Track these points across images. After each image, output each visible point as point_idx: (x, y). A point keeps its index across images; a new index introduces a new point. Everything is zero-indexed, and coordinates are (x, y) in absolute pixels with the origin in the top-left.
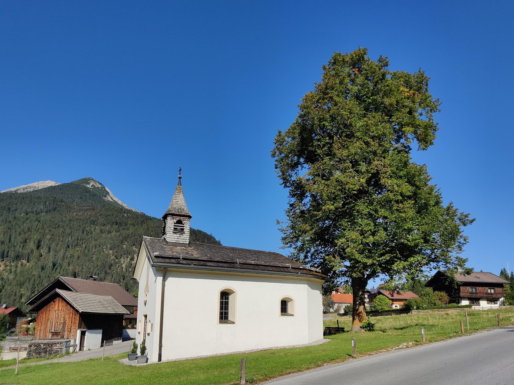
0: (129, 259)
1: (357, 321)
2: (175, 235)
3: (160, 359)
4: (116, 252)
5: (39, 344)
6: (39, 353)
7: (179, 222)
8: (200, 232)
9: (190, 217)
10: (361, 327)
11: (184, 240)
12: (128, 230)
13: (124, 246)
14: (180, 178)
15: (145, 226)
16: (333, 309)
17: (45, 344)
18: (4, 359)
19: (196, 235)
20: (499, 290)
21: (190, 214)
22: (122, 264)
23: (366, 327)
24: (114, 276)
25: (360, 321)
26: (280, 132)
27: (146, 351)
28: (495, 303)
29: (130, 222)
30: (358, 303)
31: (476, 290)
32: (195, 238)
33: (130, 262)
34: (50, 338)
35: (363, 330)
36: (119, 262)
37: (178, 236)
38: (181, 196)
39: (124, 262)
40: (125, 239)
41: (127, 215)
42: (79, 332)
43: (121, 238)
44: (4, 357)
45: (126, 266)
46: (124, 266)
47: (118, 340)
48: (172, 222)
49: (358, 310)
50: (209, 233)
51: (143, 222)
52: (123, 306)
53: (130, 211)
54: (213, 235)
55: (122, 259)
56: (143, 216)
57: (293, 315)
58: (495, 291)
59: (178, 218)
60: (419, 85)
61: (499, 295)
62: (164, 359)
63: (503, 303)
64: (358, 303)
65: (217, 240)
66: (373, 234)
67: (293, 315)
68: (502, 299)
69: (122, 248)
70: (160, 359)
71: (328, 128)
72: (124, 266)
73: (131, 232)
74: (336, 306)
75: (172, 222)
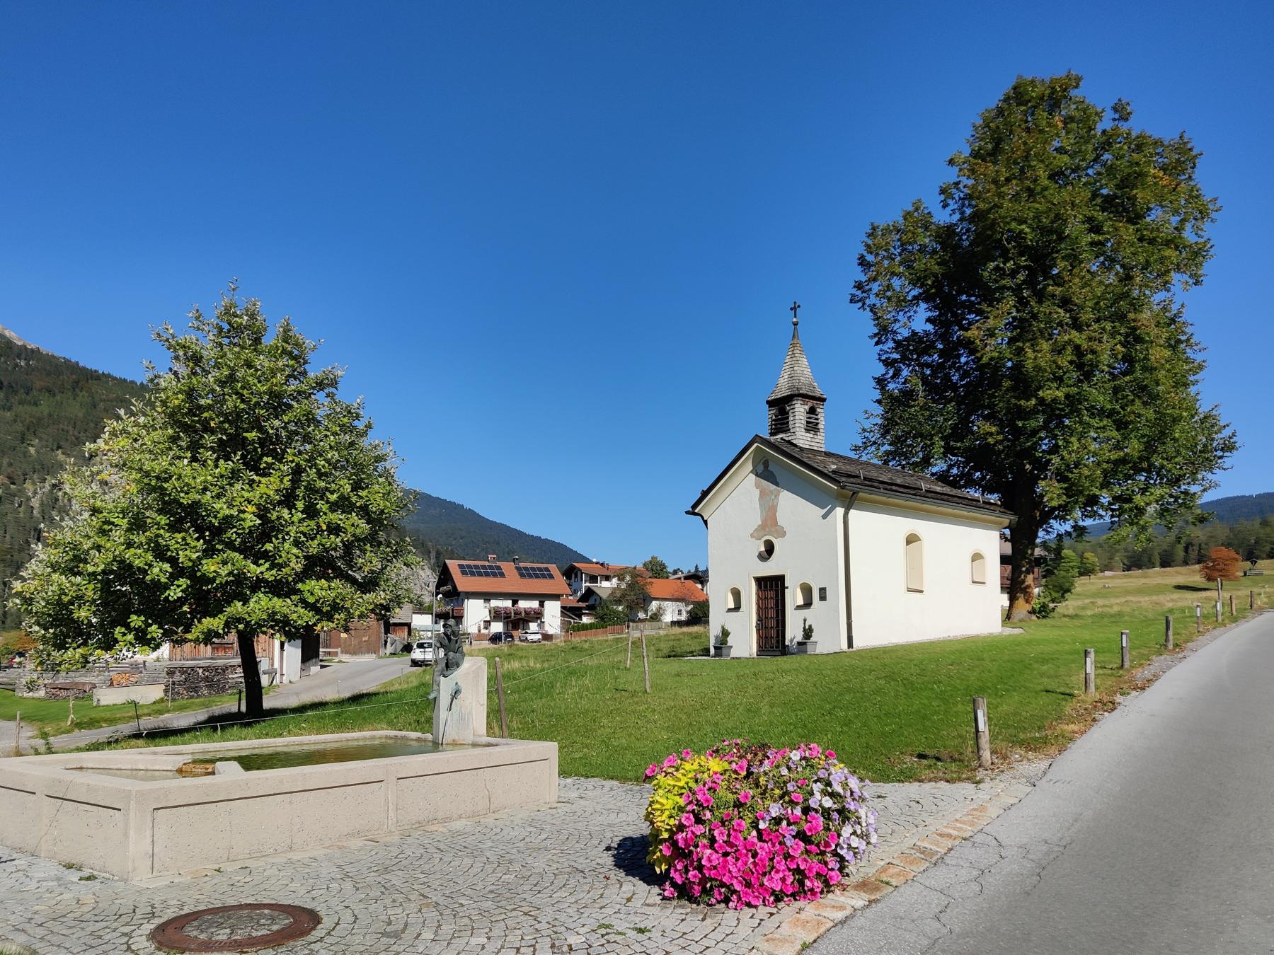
0: (47, 486)
1: (1021, 602)
3: (850, 645)
4: (10, 465)
5: (192, 669)
6: (196, 690)
7: (812, 411)
9: (824, 400)
12: (36, 404)
13: (32, 450)
14: (795, 324)
15: (83, 396)
16: (646, 612)
17: (206, 669)
18: (102, 703)
21: (819, 392)
22: (29, 499)
23: (1040, 612)
24: (10, 531)
25: (1027, 601)
29: (38, 384)
33: (51, 492)
34: (209, 654)
35: (1034, 617)
36: (22, 492)
39: (35, 493)
40: (33, 428)
41: (28, 364)
42: (277, 644)
43: (19, 427)
44: (101, 698)
45: (42, 504)
46: (35, 502)
49: (1023, 581)
51: (76, 385)
53: (35, 353)
55: (28, 486)
56: (74, 368)
60: (1181, 160)
62: (857, 644)
69: (26, 454)
70: (850, 645)
72: (35, 502)
73: (46, 413)
74: (654, 604)
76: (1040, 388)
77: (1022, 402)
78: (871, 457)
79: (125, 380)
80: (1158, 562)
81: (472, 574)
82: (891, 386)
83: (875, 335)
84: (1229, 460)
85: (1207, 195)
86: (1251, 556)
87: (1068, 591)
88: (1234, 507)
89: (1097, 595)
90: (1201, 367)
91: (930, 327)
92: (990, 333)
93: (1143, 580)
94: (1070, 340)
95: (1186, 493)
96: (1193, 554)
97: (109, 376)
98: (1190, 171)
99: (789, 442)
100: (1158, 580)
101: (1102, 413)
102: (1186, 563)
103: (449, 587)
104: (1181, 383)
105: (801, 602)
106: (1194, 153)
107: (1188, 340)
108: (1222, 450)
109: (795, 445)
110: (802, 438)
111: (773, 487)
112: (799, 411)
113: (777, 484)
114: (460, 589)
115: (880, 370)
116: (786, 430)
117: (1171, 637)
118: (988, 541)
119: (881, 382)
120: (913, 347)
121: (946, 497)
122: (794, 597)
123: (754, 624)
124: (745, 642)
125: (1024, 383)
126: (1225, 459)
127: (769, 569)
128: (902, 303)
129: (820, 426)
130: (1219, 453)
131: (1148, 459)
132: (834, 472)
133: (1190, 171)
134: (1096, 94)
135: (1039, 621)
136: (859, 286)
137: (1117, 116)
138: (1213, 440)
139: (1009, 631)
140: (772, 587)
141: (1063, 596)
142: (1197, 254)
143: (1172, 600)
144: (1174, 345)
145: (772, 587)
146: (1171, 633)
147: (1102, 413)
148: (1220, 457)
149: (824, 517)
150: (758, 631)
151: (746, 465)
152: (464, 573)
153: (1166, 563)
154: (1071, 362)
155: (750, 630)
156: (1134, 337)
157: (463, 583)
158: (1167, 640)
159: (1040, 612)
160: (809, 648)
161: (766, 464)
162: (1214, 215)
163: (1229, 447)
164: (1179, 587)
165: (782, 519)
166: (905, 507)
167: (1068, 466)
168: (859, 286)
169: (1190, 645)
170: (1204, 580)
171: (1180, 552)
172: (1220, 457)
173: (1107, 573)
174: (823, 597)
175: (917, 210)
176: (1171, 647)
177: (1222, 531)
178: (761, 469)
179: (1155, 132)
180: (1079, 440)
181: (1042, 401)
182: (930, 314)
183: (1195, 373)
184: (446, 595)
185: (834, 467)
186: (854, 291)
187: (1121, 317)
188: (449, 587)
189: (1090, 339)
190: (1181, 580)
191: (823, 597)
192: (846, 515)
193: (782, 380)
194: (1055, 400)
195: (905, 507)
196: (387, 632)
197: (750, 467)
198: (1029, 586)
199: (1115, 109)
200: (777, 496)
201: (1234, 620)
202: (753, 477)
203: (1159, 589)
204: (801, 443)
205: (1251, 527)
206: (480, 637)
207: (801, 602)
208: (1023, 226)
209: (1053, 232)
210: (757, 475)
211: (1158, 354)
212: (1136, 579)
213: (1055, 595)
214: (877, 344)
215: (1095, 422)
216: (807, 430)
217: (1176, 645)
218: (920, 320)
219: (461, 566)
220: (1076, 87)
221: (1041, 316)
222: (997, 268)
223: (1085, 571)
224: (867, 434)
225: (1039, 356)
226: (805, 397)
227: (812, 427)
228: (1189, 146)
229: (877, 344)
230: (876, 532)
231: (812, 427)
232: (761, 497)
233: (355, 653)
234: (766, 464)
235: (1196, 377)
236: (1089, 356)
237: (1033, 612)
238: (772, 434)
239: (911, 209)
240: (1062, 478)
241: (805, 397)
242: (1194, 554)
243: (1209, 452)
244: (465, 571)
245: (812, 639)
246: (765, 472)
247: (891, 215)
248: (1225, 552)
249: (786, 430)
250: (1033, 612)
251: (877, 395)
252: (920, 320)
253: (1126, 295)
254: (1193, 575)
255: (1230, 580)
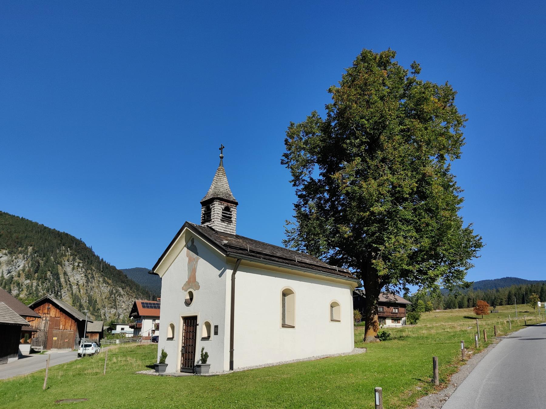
2: (223, 224)
3: (231, 368)
7: (227, 209)
8: (67, 235)
9: (236, 204)
10: (376, 337)
11: (232, 231)
14: (222, 158)
19: (62, 239)
20: (402, 310)
21: (233, 198)
23: (381, 337)
25: (375, 330)
26: (292, 125)
27: (208, 359)
28: (398, 323)
30: (372, 312)
31: (383, 310)
32: (59, 242)
35: (378, 340)
37: (226, 224)
38: (225, 179)
47: (14, 357)
48: (220, 208)
49: (373, 319)
50: (78, 237)
52: (22, 316)
54: (83, 240)
57: (340, 321)
58: (398, 311)
59: (226, 204)
60: (447, 96)
61: (402, 315)
63: (405, 323)
64: (372, 312)
65: (88, 245)
66: (416, 241)
67: (340, 321)
68: (403, 319)
70: (231, 368)
71: (367, 126)
75: (220, 208)
76: (372, 206)
77: (362, 213)
78: (291, 247)
79: (14, 216)
80: (457, 306)
81: (148, 307)
82: (303, 209)
83: (293, 181)
84: (479, 252)
85: (460, 114)
86: (493, 304)
87: (417, 319)
88: (485, 285)
89: (432, 320)
90: (461, 200)
91: (321, 178)
92: (345, 174)
93: (451, 314)
94: (388, 179)
95: (458, 271)
96: (471, 303)
97: (7, 214)
98: (451, 101)
99: (211, 228)
100: (457, 314)
101: (407, 222)
102: (468, 307)
103: (136, 313)
104: (452, 207)
105: (206, 335)
106: (453, 91)
107: (454, 185)
108: (475, 247)
109: (213, 230)
110: (217, 224)
111: (195, 256)
112: (217, 209)
113: (197, 254)
114: (140, 315)
115: (296, 200)
116: (209, 220)
117: (437, 375)
118: (343, 295)
119: (297, 206)
120: (312, 189)
121: (331, 269)
122: (202, 331)
123: (180, 348)
124: (174, 364)
125: (363, 203)
126: (477, 252)
127: (189, 312)
128: (306, 164)
129: (232, 219)
130: (473, 249)
131: (435, 250)
132: (225, 245)
133: (451, 101)
134: (402, 62)
135: (380, 343)
136: (286, 156)
137: (413, 71)
138: (470, 241)
139: (361, 351)
140: (191, 322)
141: (415, 321)
142: (457, 142)
143: (460, 325)
144: (446, 187)
145: (191, 322)
146: (437, 371)
147: (407, 222)
148: (474, 251)
149: (220, 276)
150: (183, 354)
151: (182, 242)
152: (144, 307)
153: (460, 307)
154: (389, 192)
155: (178, 354)
156: (424, 180)
157: (142, 311)
158: (434, 377)
159: (381, 337)
160: (203, 369)
161: (193, 242)
162: (464, 123)
163: (478, 245)
164: (465, 317)
165: (199, 279)
166: (318, 278)
167: (389, 252)
168: (286, 156)
169: (455, 376)
170: (475, 314)
171: (466, 303)
172: (474, 251)
173: (437, 310)
174: (216, 333)
175: (314, 116)
176: (437, 383)
177: (481, 294)
178: (190, 244)
179: (433, 81)
180: (395, 236)
181: (372, 213)
182: (322, 171)
183: (458, 203)
184: (135, 317)
185: (226, 242)
186: (284, 158)
187: (415, 170)
188: (136, 313)
189: (398, 178)
190: (466, 314)
191: (216, 333)
192: (234, 274)
193: (210, 190)
194: (380, 213)
195: (318, 278)
196: (81, 336)
197: (183, 243)
198: (375, 322)
199: (412, 67)
200: (197, 262)
201: (486, 345)
202: (185, 249)
203: (456, 319)
204: (217, 228)
205: (493, 293)
206: (146, 338)
207: (206, 335)
208: (364, 120)
209: (381, 125)
210: (188, 248)
211: (436, 189)
212: (449, 313)
213: (412, 321)
214: (294, 185)
215: (404, 227)
216: (222, 221)
217: (442, 381)
218: (316, 173)
219: (142, 303)
220: (393, 57)
221: (372, 167)
222: (351, 143)
223: (428, 310)
224: (290, 234)
225: (370, 187)
226: (221, 200)
227: (227, 218)
228: (451, 88)
229: (294, 185)
230: (257, 289)
231: (227, 218)
232: (189, 263)
233: (60, 348)
234: (193, 242)
235: (459, 206)
236: (398, 189)
237: (377, 337)
238: (203, 223)
239: (311, 116)
240: (385, 258)
241: (221, 200)
242: (471, 303)
243: (468, 246)
244: (144, 305)
245: (208, 363)
246: (192, 247)
247: (302, 119)
248: (483, 303)
249: (209, 220)
250: (377, 337)
251: (295, 213)
252: (316, 173)
253: (419, 158)
254: (470, 312)
255: (485, 314)
